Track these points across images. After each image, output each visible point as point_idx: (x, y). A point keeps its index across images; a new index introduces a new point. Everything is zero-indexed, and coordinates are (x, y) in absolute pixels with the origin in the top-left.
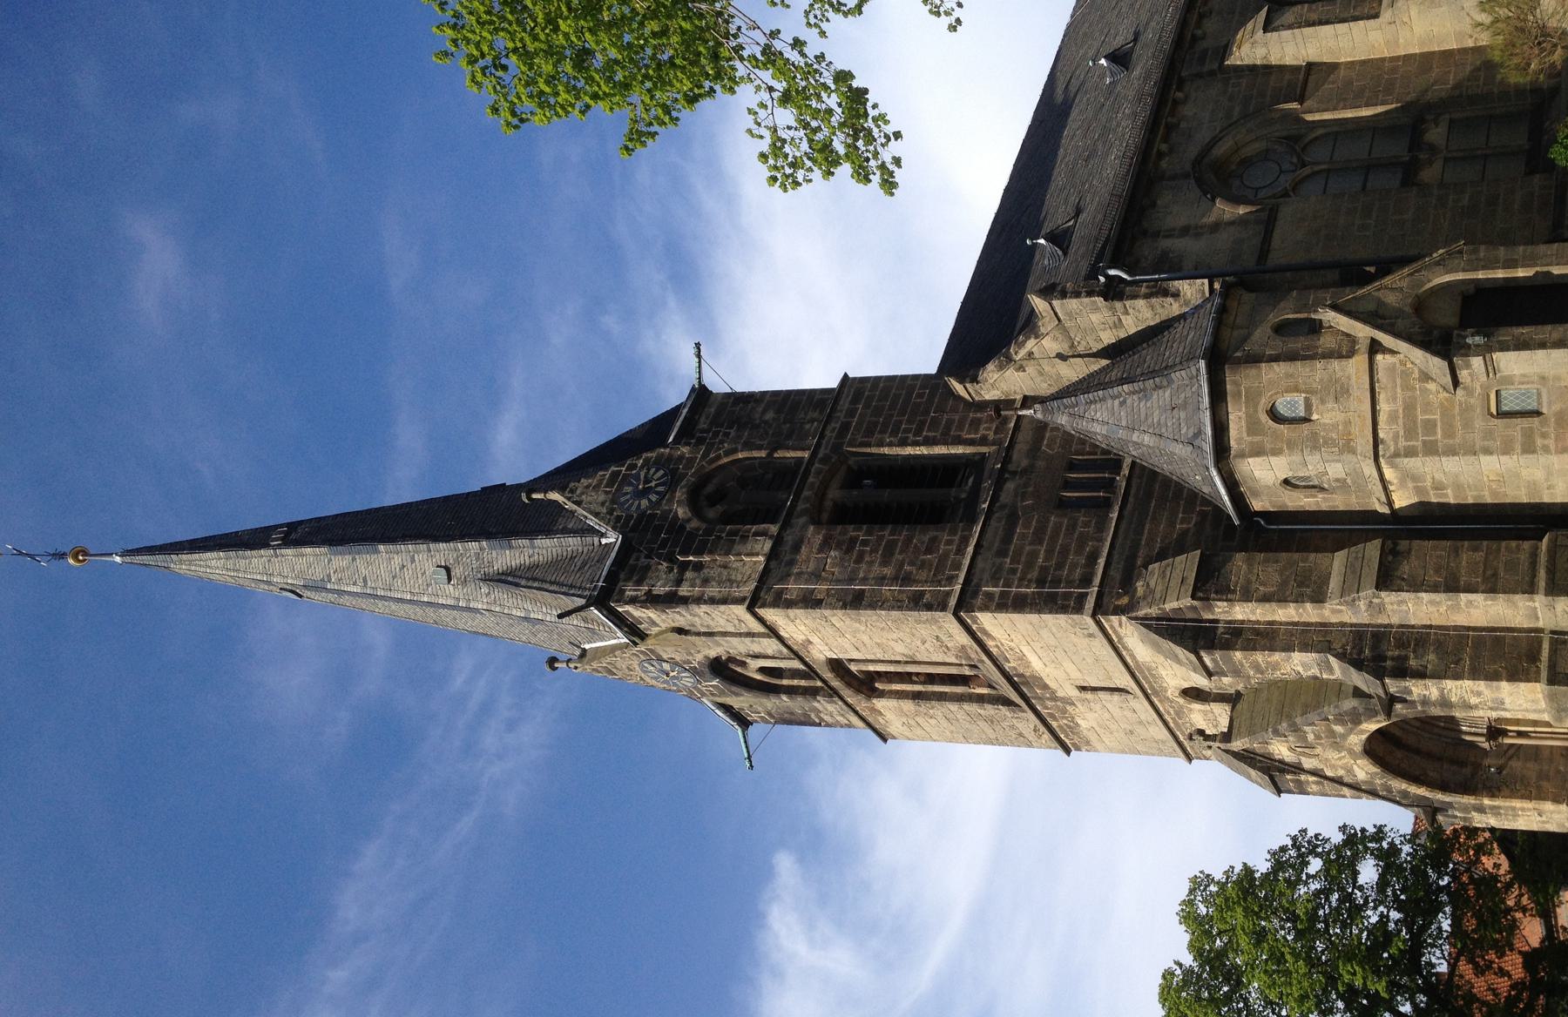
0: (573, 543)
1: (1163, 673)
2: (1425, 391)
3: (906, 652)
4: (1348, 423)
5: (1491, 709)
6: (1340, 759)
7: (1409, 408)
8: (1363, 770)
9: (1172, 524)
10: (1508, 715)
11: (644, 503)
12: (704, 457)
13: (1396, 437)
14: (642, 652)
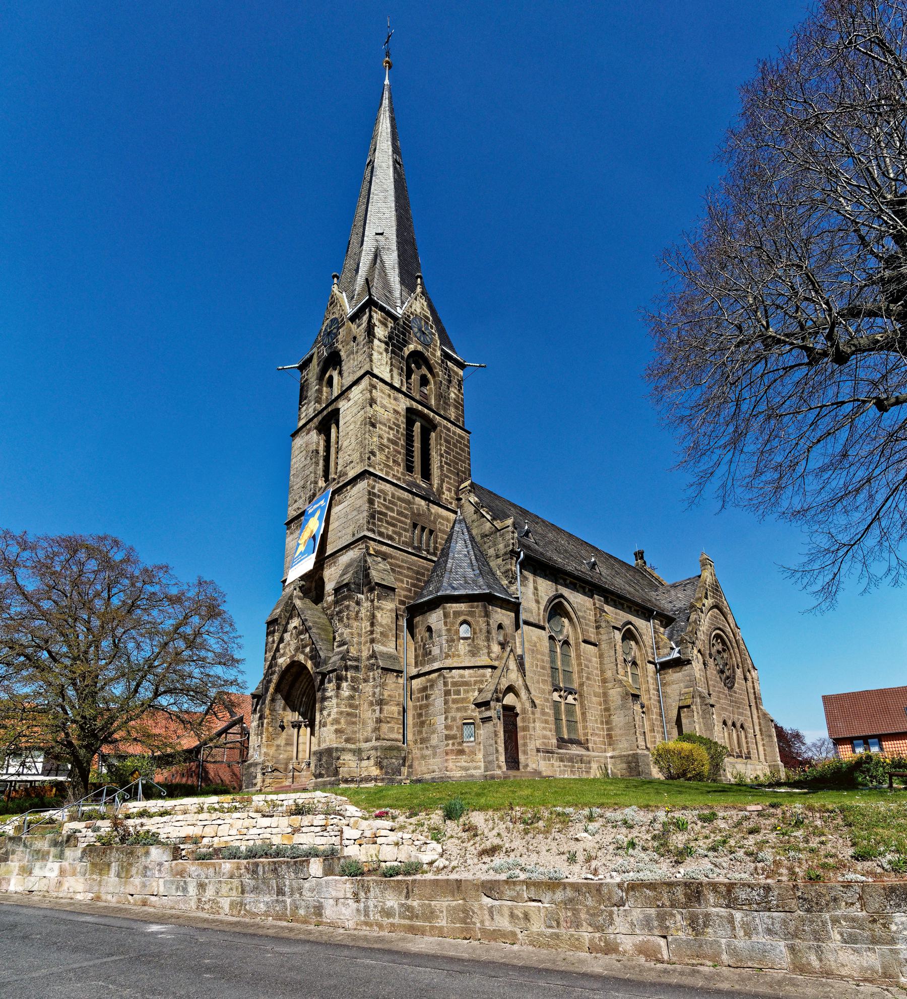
0: (397, 294)
1: (333, 569)
2: (474, 691)
3: (344, 446)
4: (459, 656)
5: (320, 721)
6: (290, 651)
7: (466, 684)
8: (283, 661)
9: (407, 576)
10: (317, 728)
11: (416, 330)
12: (435, 361)
13: (452, 677)
14: (343, 319)
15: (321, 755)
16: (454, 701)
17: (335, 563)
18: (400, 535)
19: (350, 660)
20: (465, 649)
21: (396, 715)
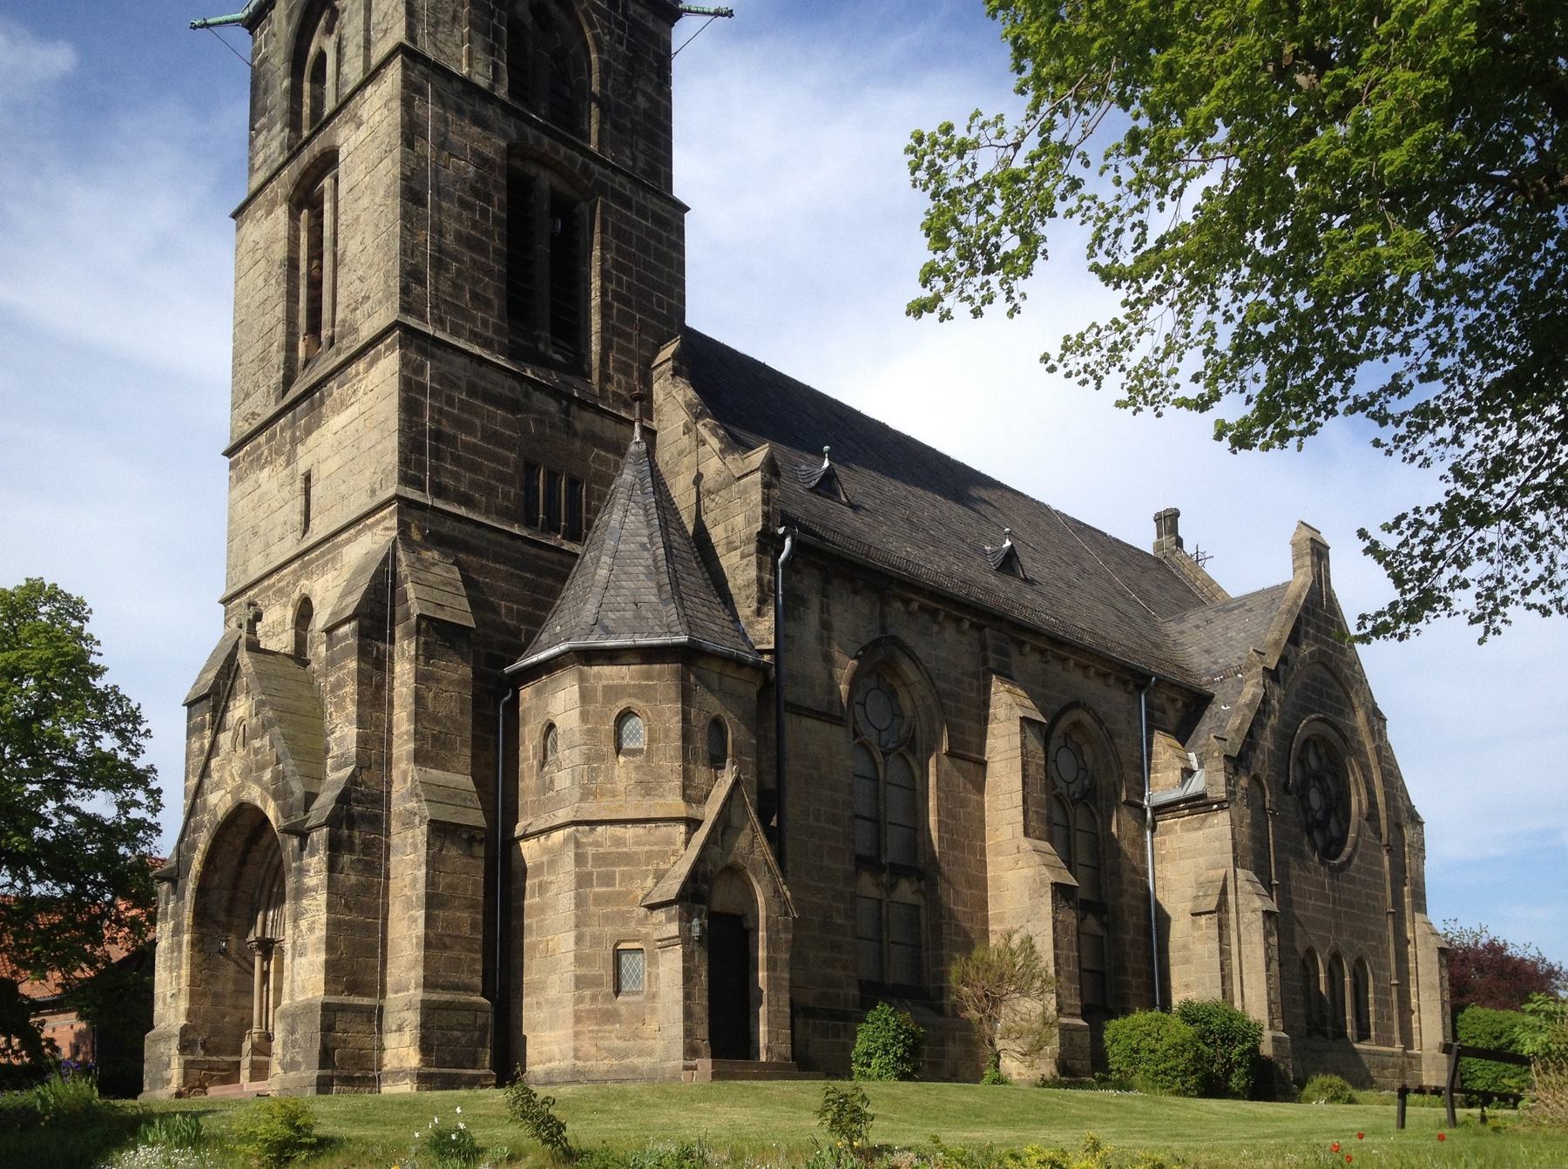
1: (329, 576)
2: (645, 875)
3: (349, 254)
4: (614, 794)
5: (294, 943)
6: (232, 775)
7: (628, 859)
9: (506, 596)
13: (597, 844)
15: (294, 1020)
16: (600, 900)
17: (333, 560)
18: (489, 491)
19: (359, 802)
20: (629, 778)
21: (466, 930)
